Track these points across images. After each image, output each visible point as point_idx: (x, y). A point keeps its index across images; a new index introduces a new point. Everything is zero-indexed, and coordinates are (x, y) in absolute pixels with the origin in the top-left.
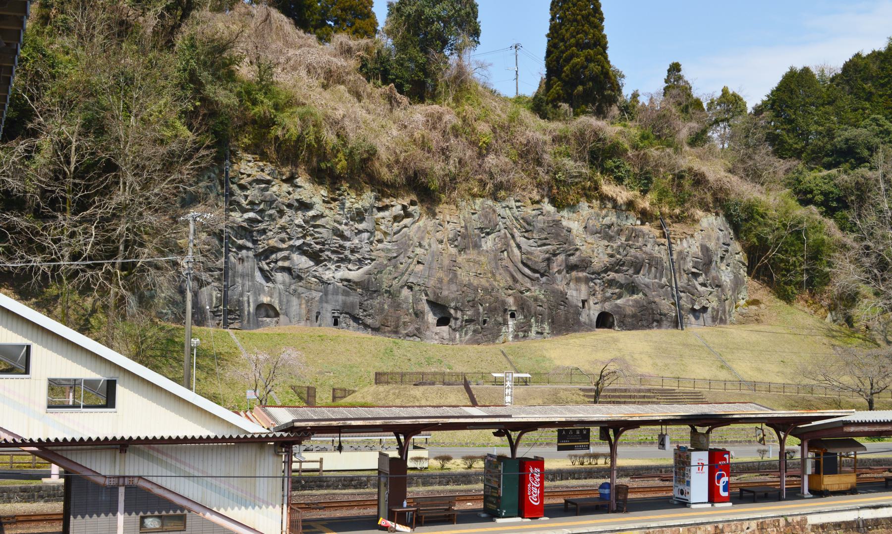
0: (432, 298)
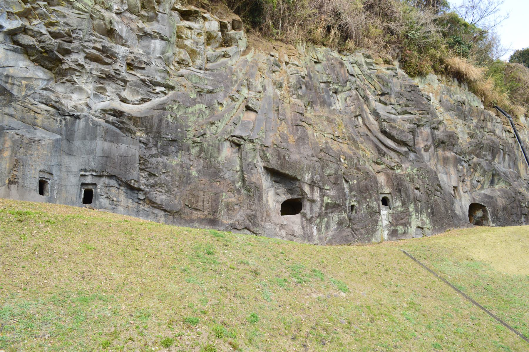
0: (274, 164)
